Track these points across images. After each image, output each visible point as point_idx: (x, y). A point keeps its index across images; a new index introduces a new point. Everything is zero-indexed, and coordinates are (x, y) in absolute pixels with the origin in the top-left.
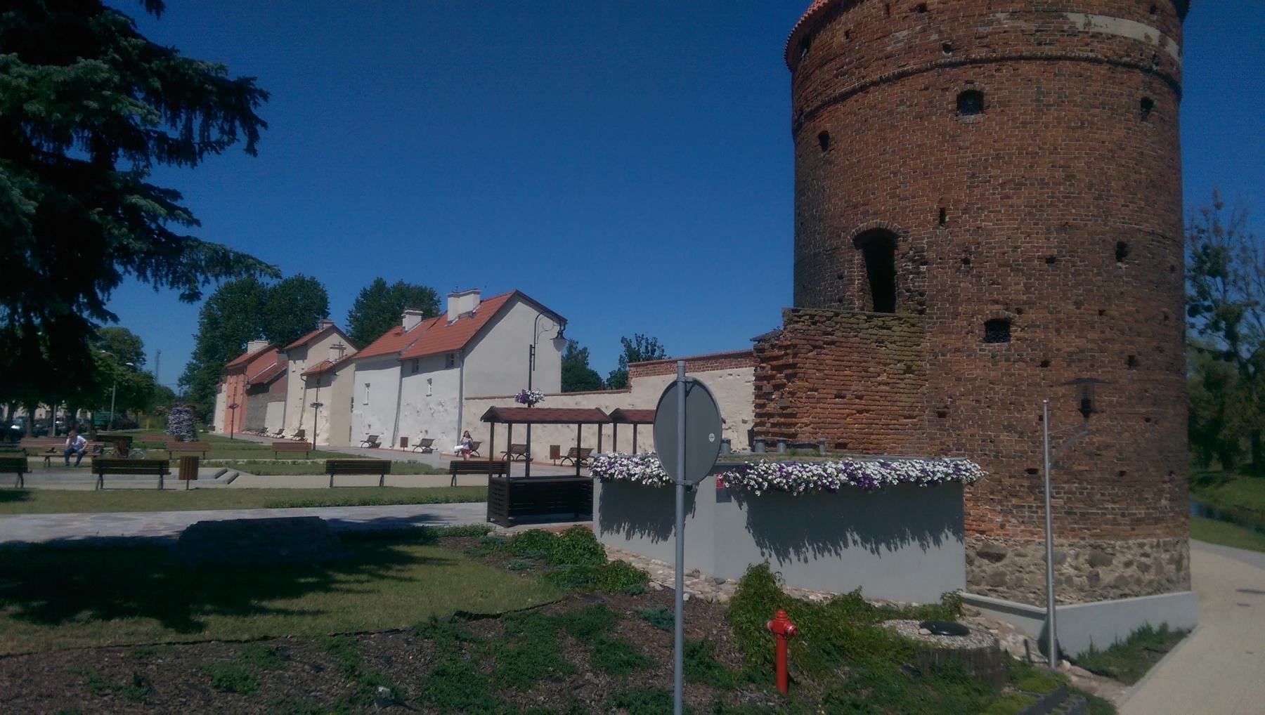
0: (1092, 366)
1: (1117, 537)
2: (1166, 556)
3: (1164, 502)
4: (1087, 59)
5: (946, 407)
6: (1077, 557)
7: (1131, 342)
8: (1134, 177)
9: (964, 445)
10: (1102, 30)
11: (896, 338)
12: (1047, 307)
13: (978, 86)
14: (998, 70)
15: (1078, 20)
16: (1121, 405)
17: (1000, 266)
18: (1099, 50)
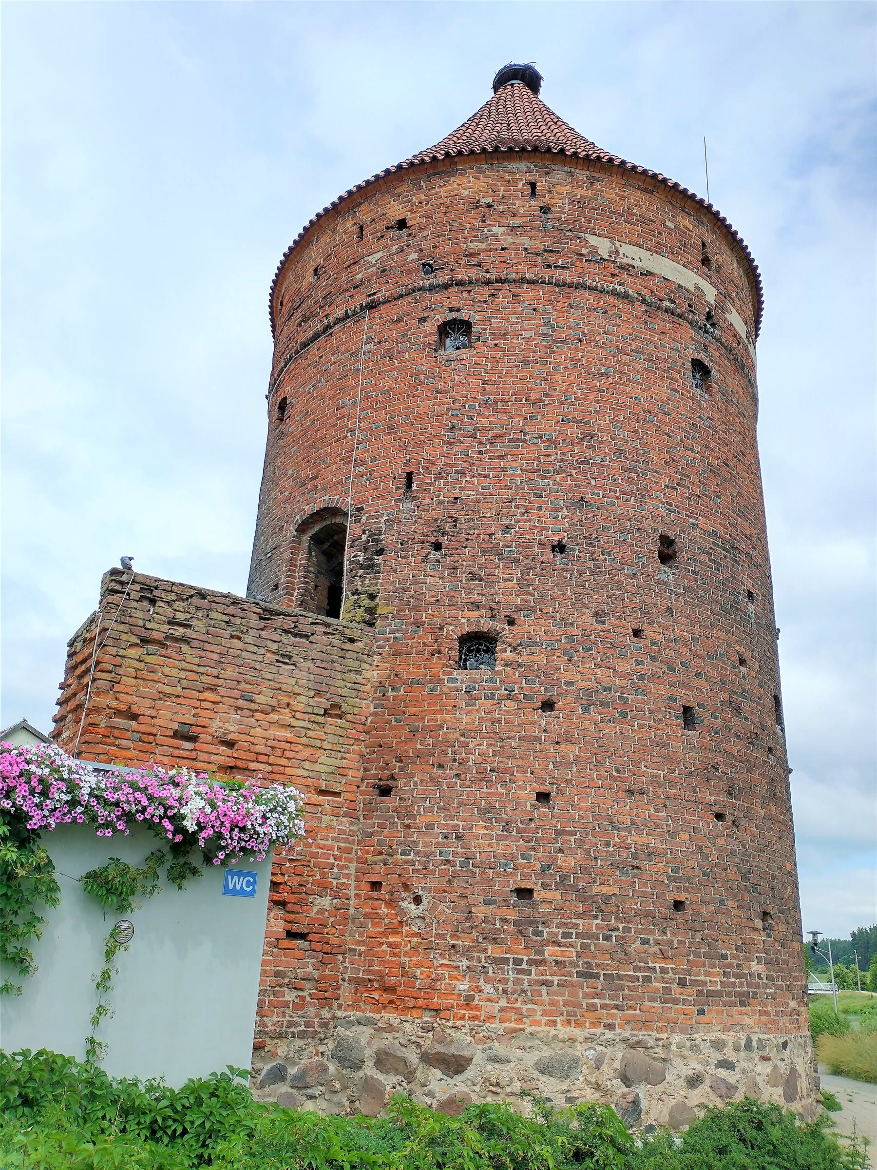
1: (673, 1026)
2: (765, 1069)
3: (756, 967)
4: (614, 293)
5: (392, 777)
7: (685, 686)
9: (416, 843)
16: (673, 784)
17: (484, 552)
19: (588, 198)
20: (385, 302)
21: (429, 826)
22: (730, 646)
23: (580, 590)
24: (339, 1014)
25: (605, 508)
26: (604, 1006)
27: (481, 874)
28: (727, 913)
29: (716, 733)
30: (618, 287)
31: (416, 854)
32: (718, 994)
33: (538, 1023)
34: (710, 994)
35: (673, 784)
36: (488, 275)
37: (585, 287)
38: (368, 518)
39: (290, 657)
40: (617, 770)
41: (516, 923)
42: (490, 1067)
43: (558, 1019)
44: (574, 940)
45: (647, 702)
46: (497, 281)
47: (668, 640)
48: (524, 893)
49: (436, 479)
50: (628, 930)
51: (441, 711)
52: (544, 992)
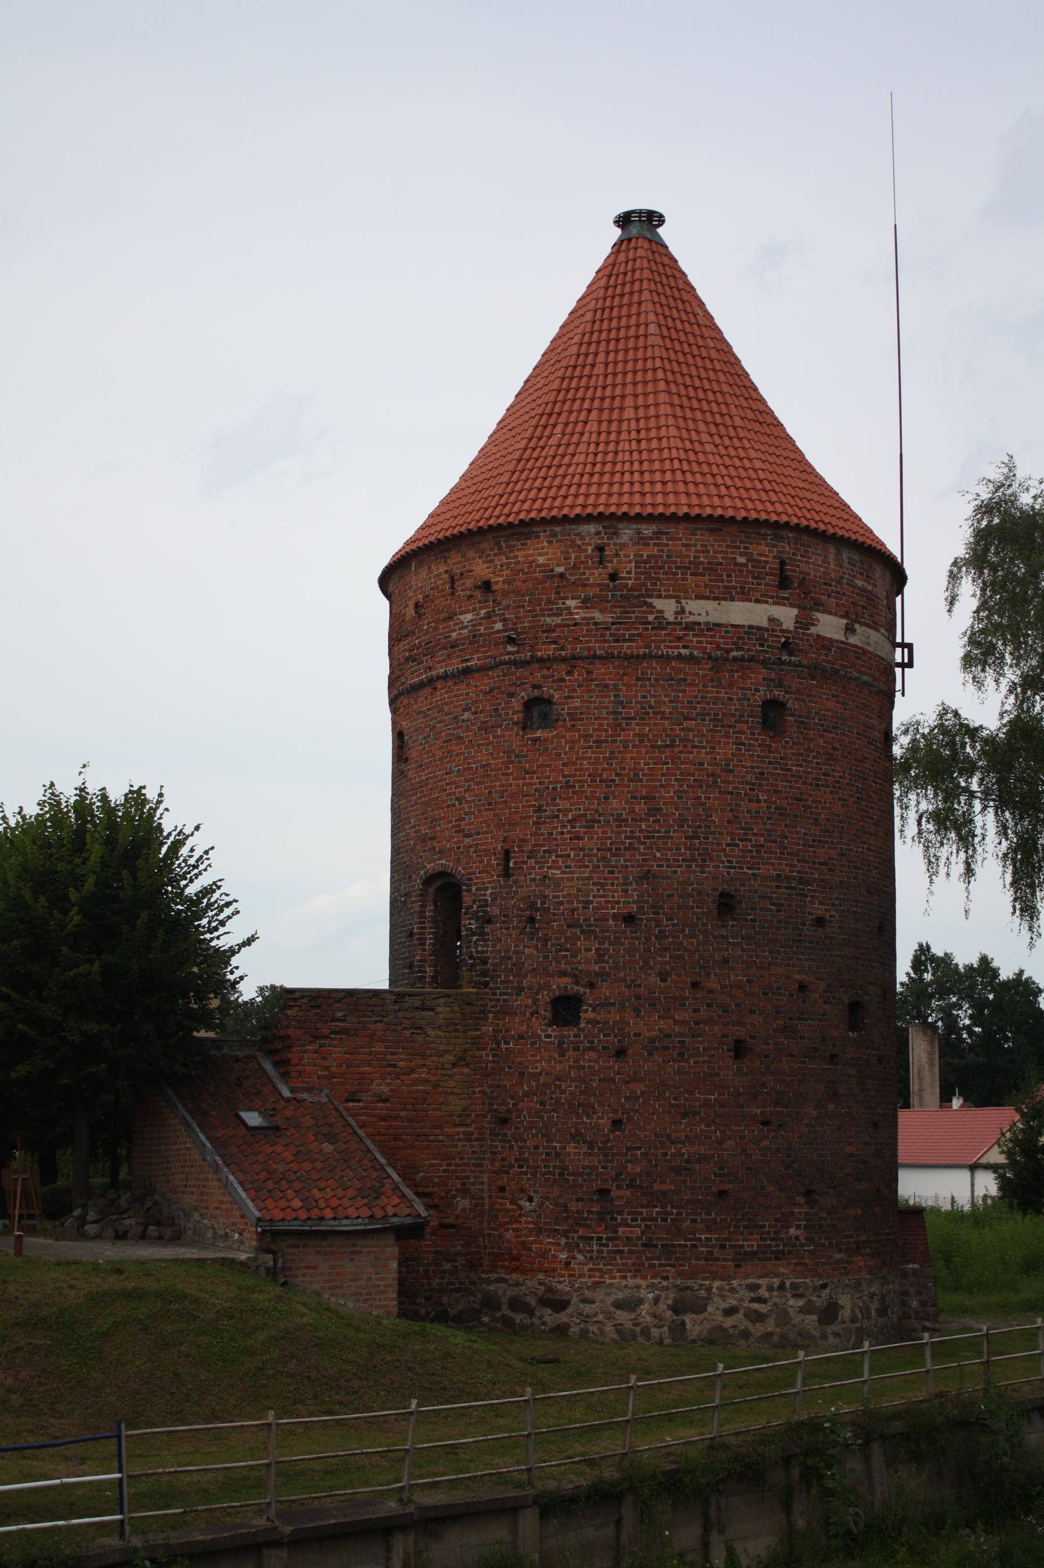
0: (681, 1055)
4: (680, 657)
9: (527, 1160)
10: (702, 619)
12: (624, 980)
14: (569, 673)
15: (668, 607)
17: (569, 926)
19: (654, 556)
21: (536, 1147)
24: (483, 1276)
26: (660, 1265)
27: (573, 1180)
29: (766, 1056)
30: (683, 651)
31: (528, 1167)
32: (755, 1253)
33: (614, 1278)
36: (563, 653)
38: (478, 889)
39: (421, 1028)
40: (675, 1099)
41: (598, 1213)
42: (582, 1306)
43: (629, 1275)
44: (639, 1222)
47: (724, 987)
48: (604, 1192)
49: (529, 857)
50: (681, 1214)
51: (540, 1061)
52: (618, 1258)
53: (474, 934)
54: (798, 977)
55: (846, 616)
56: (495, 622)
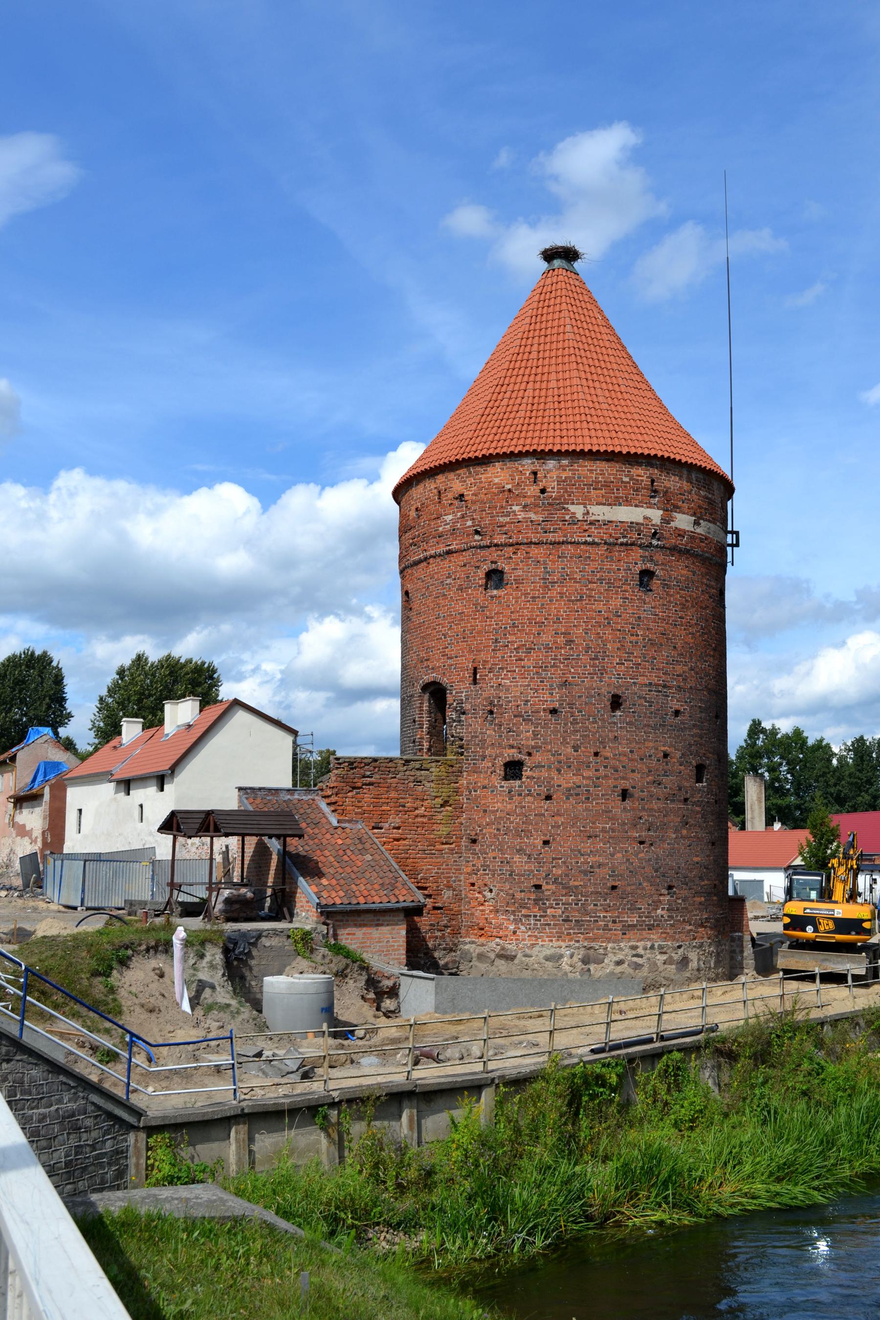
1: (609, 940)
4: (586, 543)
6: (572, 956)
7: (624, 778)
8: (628, 638)
9: (488, 866)
10: (600, 518)
11: (433, 778)
12: (550, 751)
13: (500, 565)
14: (514, 553)
17: (515, 716)
18: (595, 535)
20: (456, 552)
21: (494, 858)
22: (657, 749)
23: (565, 735)
25: (579, 685)
28: (643, 889)
32: (634, 926)
34: (629, 926)
35: (613, 830)
37: (568, 543)
38: (456, 693)
41: (534, 900)
42: (524, 959)
45: (601, 791)
46: (517, 544)
47: (615, 755)
48: (538, 887)
51: (497, 802)
53: (454, 721)
54: (663, 749)
55: (694, 514)
56: (467, 521)
